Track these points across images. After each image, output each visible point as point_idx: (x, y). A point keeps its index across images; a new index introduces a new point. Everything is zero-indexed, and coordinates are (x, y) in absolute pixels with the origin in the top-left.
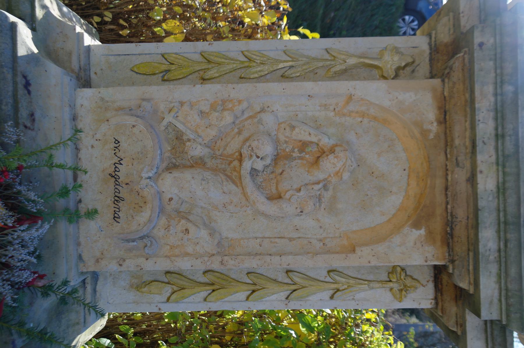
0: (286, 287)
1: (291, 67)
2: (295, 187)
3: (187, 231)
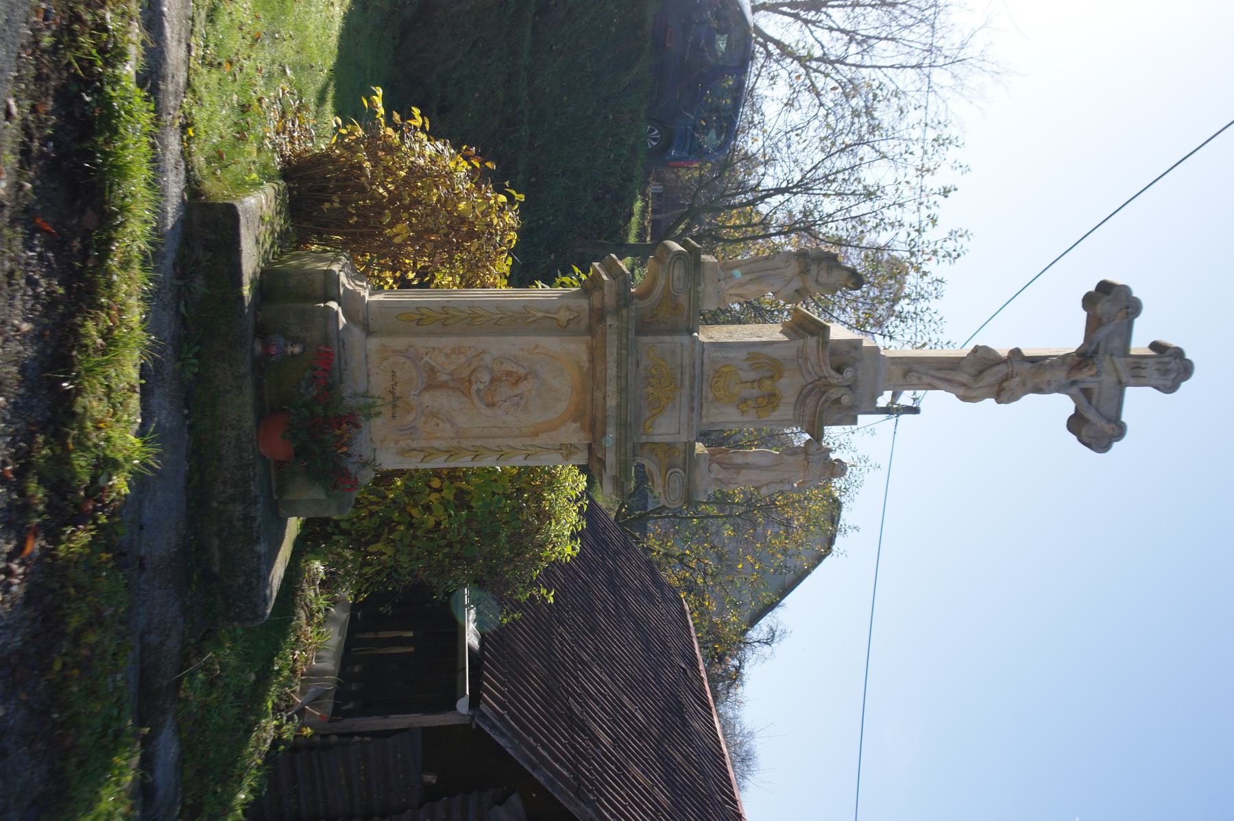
0: (497, 453)
1: (502, 318)
2: (503, 399)
3: (438, 425)
